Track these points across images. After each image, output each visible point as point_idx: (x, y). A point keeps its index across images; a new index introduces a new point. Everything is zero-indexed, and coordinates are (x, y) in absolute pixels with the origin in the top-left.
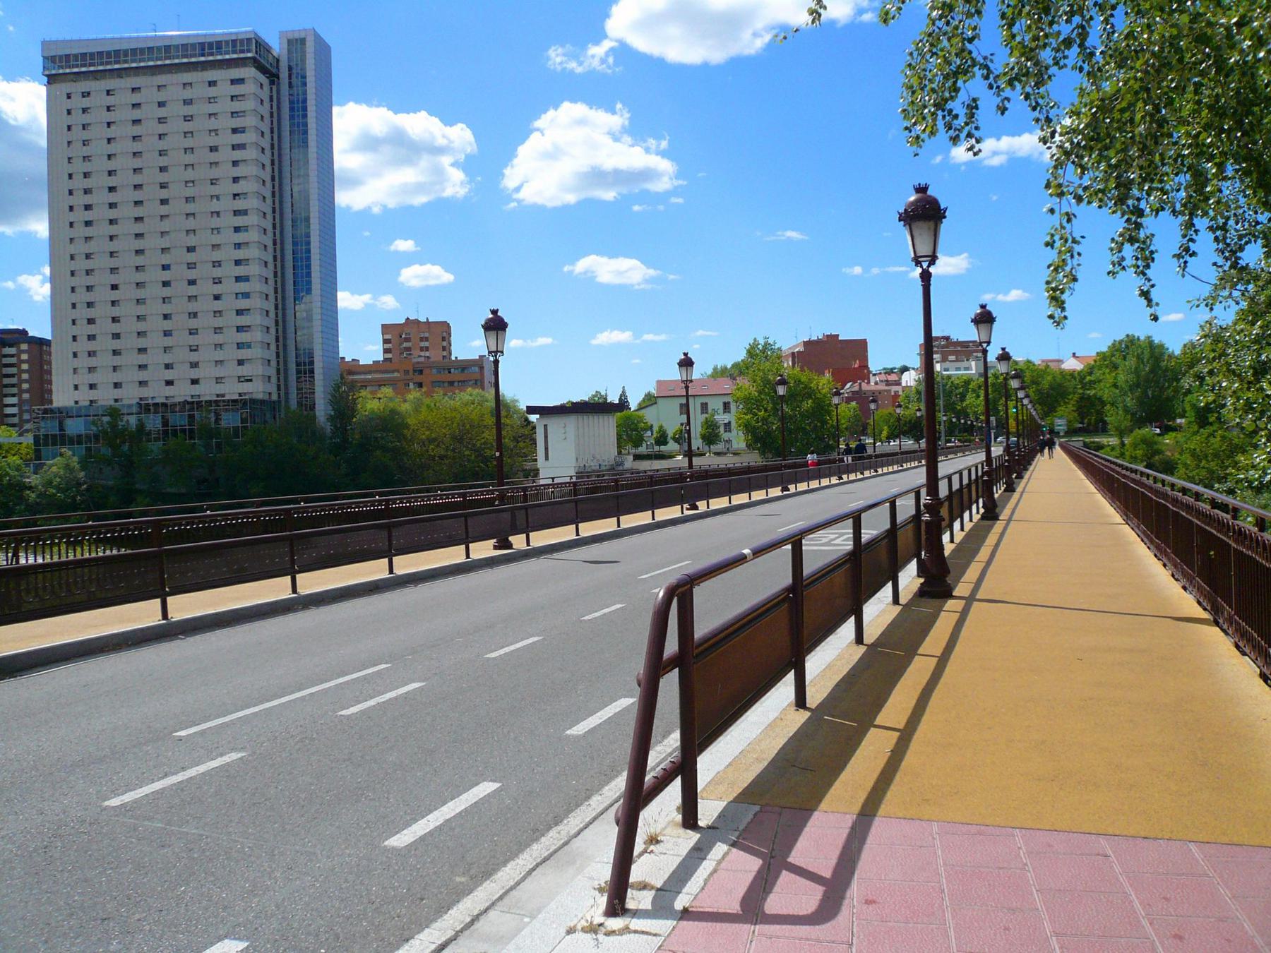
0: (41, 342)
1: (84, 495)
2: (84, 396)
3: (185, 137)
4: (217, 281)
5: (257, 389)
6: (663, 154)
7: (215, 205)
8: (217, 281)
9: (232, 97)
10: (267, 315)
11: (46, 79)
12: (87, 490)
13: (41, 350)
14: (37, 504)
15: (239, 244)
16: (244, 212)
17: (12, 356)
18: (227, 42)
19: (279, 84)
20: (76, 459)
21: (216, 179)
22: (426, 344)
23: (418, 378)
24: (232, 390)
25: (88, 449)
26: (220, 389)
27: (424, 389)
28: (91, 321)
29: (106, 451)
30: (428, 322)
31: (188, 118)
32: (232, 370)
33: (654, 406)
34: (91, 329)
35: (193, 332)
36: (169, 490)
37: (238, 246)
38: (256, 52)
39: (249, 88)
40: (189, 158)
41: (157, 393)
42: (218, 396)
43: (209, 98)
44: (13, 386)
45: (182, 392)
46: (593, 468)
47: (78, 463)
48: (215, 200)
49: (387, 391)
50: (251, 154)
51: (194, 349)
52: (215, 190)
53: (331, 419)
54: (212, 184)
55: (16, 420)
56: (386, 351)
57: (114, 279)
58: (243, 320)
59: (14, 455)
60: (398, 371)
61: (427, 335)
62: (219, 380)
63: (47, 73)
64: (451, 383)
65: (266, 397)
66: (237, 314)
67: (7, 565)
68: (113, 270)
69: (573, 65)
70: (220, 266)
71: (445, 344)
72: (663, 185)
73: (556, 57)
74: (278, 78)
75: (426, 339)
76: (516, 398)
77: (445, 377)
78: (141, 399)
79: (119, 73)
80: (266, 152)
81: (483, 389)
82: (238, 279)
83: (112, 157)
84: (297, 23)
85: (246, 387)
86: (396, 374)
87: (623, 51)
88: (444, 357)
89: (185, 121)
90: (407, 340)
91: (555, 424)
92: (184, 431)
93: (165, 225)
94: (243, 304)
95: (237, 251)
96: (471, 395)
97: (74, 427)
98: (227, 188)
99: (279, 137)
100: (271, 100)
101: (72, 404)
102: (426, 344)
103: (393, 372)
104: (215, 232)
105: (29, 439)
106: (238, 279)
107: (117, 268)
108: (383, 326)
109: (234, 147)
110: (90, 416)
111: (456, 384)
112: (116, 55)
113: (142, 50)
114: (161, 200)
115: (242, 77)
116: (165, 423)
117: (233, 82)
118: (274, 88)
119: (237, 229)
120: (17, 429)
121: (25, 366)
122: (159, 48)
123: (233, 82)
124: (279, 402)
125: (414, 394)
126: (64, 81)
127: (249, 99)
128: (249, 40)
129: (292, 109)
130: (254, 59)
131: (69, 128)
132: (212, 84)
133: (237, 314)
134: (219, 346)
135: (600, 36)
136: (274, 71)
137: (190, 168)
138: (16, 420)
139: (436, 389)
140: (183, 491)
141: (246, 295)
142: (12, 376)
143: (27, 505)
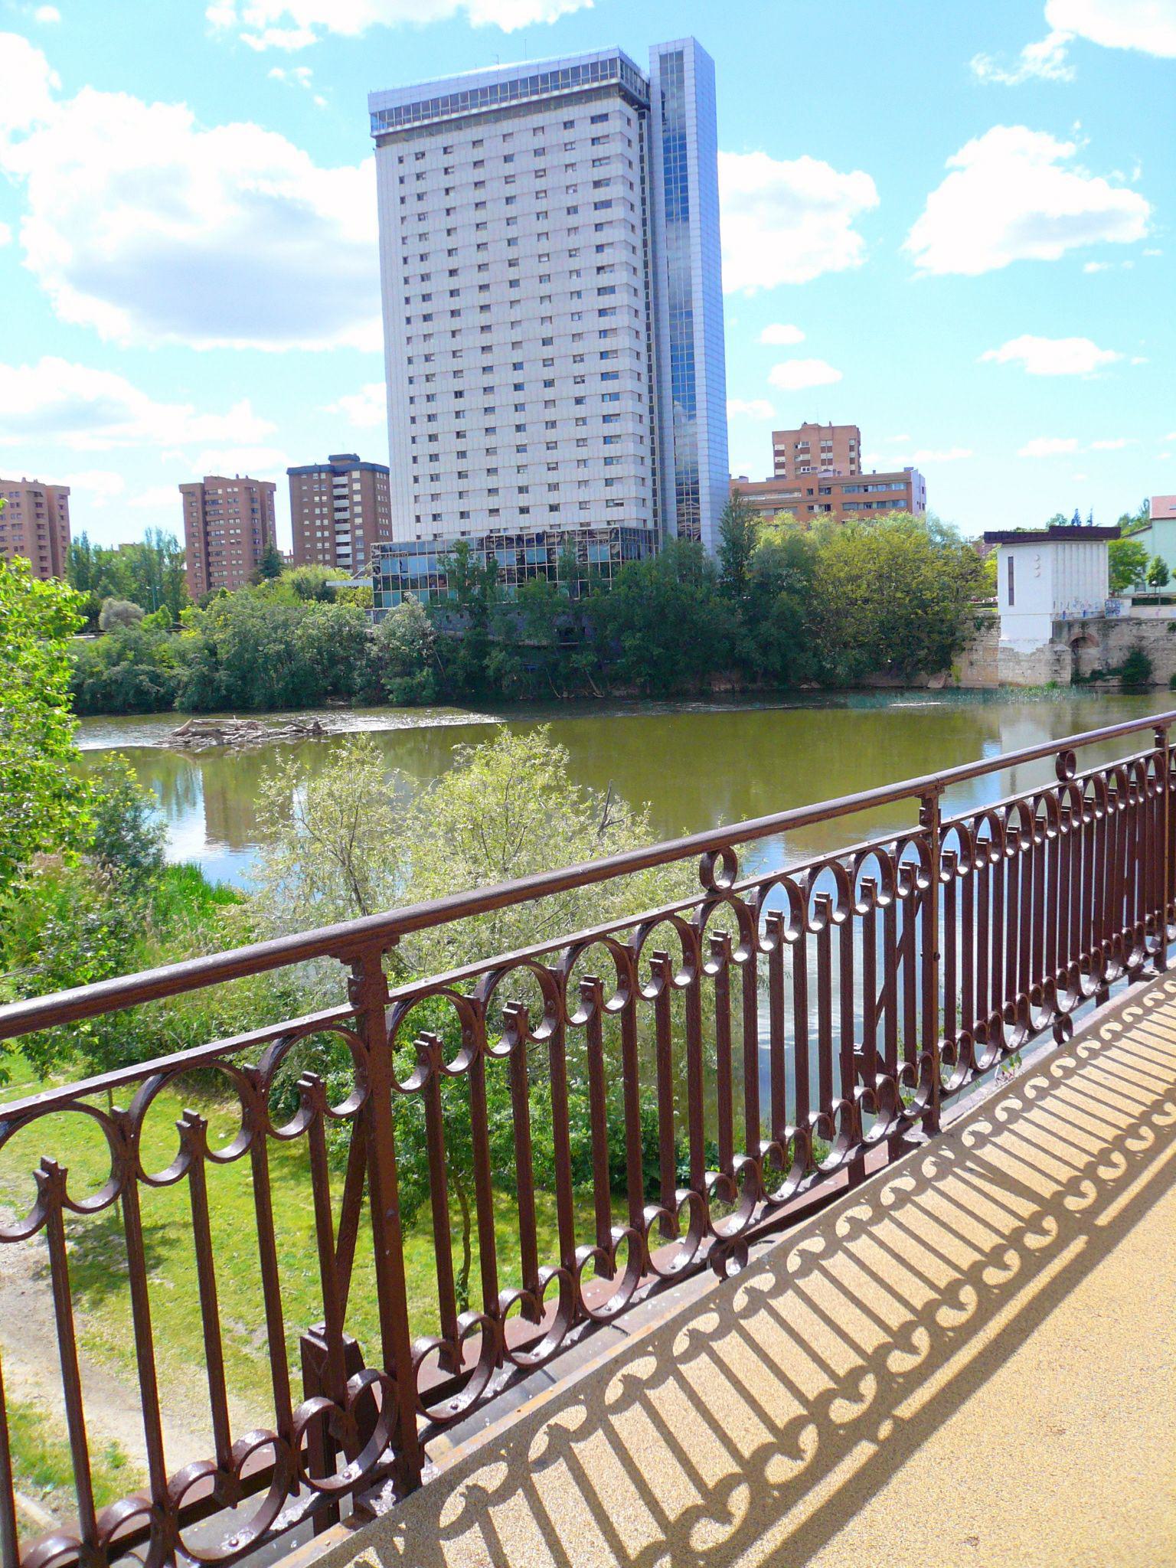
0: (373, 469)
1: (431, 648)
2: (427, 529)
3: (537, 198)
4: (580, 380)
5: (631, 516)
6: (1135, 188)
7: (576, 284)
8: (579, 380)
9: (593, 140)
10: (641, 422)
11: (374, 141)
12: (434, 642)
13: (374, 477)
14: (380, 659)
15: (605, 331)
16: (611, 290)
17: (344, 486)
18: (585, 67)
19: (650, 118)
20: (421, 604)
21: (575, 250)
22: (830, 455)
23: (826, 499)
24: (599, 518)
25: (433, 594)
26: (584, 516)
27: (833, 513)
28: (432, 438)
29: (453, 594)
30: (831, 428)
31: (540, 174)
32: (599, 492)
33: (1149, 532)
34: (434, 448)
35: (551, 446)
36: (527, 642)
37: (603, 333)
38: (622, 77)
39: (614, 125)
40: (543, 226)
41: (511, 524)
42: (582, 525)
43: (566, 145)
44: (345, 521)
45: (538, 522)
46: (1076, 616)
47: (424, 609)
48: (574, 277)
49: (786, 516)
50: (617, 212)
51: (552, 467)
52: (575, 263)
53: (722, 551)
54: (571, 256)
55: (349, 561)
56: (778, 466)
57: (457, 385)
58: (611, 429)
59: (350, 602)
60: (799, 490)
61: (830, 443)
62: (583, 505)
63: (376, 133)
64: (869, 505)
65: (641, 526)
66: (604, 421)
67: (1170, 771)
68: (457, 374)
69: (1001, 77)
70: (582, 360)
71: (853, 454)
72: (1133, 231)
73: (980, 67)
74: (649, 109)
75: (830, 449)
76: (955, 523)
77: (861, 497)
78: (491, 531)
79: (458, 124)
80: (636, 208)
81: (911, 511)
82: (605, 376)
83: (452, 232)
84: (670, 34)
85: (616, 514)
86: (796, 495)
87: (1080, 50)
88: (852, 472)
89: (537, 177)
90: (805, 451)
91: (1024, 556)
92: (542, 569)
93: (516, 314)
94: (611, 407)
95: (602, 340)
96: (895, 520)
97: (418, 567)
98: (589, 260)
99: (652, 189)
100: (641, 140)
101: (414, 539)
102: (830, 455)
103: (791, 492)
104: (576, 317)
105: (367, 582)
106: (605, 376)
107: (462, 371)
108: (775, 434)
109: (597, 206)
110: (434, 553)
111: (874, 506)
112: (454, 101)
113: (484, 91)
114: (511, 282)
115: (604, 112)
116: (521, 560)
117: (594, 120)
118: (645, 122)
119: (602, 312)
120: (351, 571)
121: (357, 498)
122: (503, 86)
123: (594, 120)
124: (656, 531)
125: (821, 520)
126: (395, 141)
127: (614, 140)
128: (613, 61)
129: (667, 150)
130: (618, 85)
131: (403, 200)
132: (568, 125)
133: (604, 421)
134: (582, 462)
135: (1042, 30)
136: (643, 99)
137: (544, 238)
138: (349, 561)
139: (850, 513)
140: (544, 643)
141: (615, 396)
142: (345, 509)
143: (368, 660)
